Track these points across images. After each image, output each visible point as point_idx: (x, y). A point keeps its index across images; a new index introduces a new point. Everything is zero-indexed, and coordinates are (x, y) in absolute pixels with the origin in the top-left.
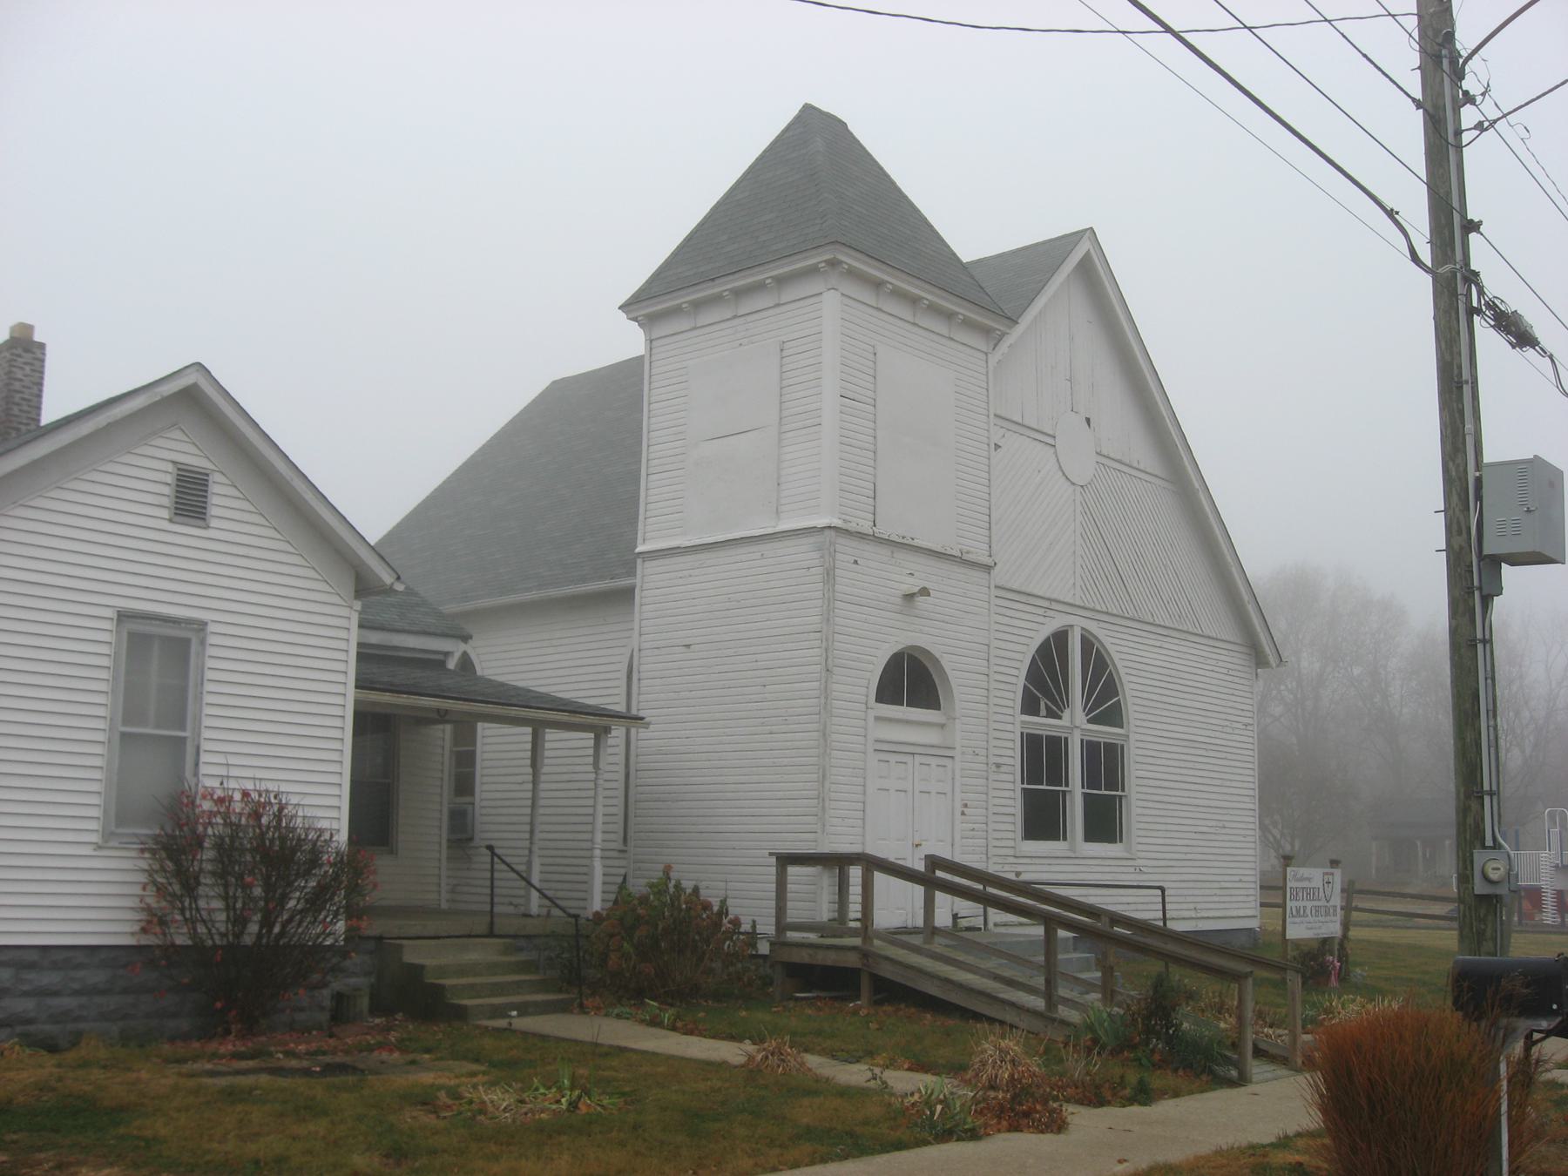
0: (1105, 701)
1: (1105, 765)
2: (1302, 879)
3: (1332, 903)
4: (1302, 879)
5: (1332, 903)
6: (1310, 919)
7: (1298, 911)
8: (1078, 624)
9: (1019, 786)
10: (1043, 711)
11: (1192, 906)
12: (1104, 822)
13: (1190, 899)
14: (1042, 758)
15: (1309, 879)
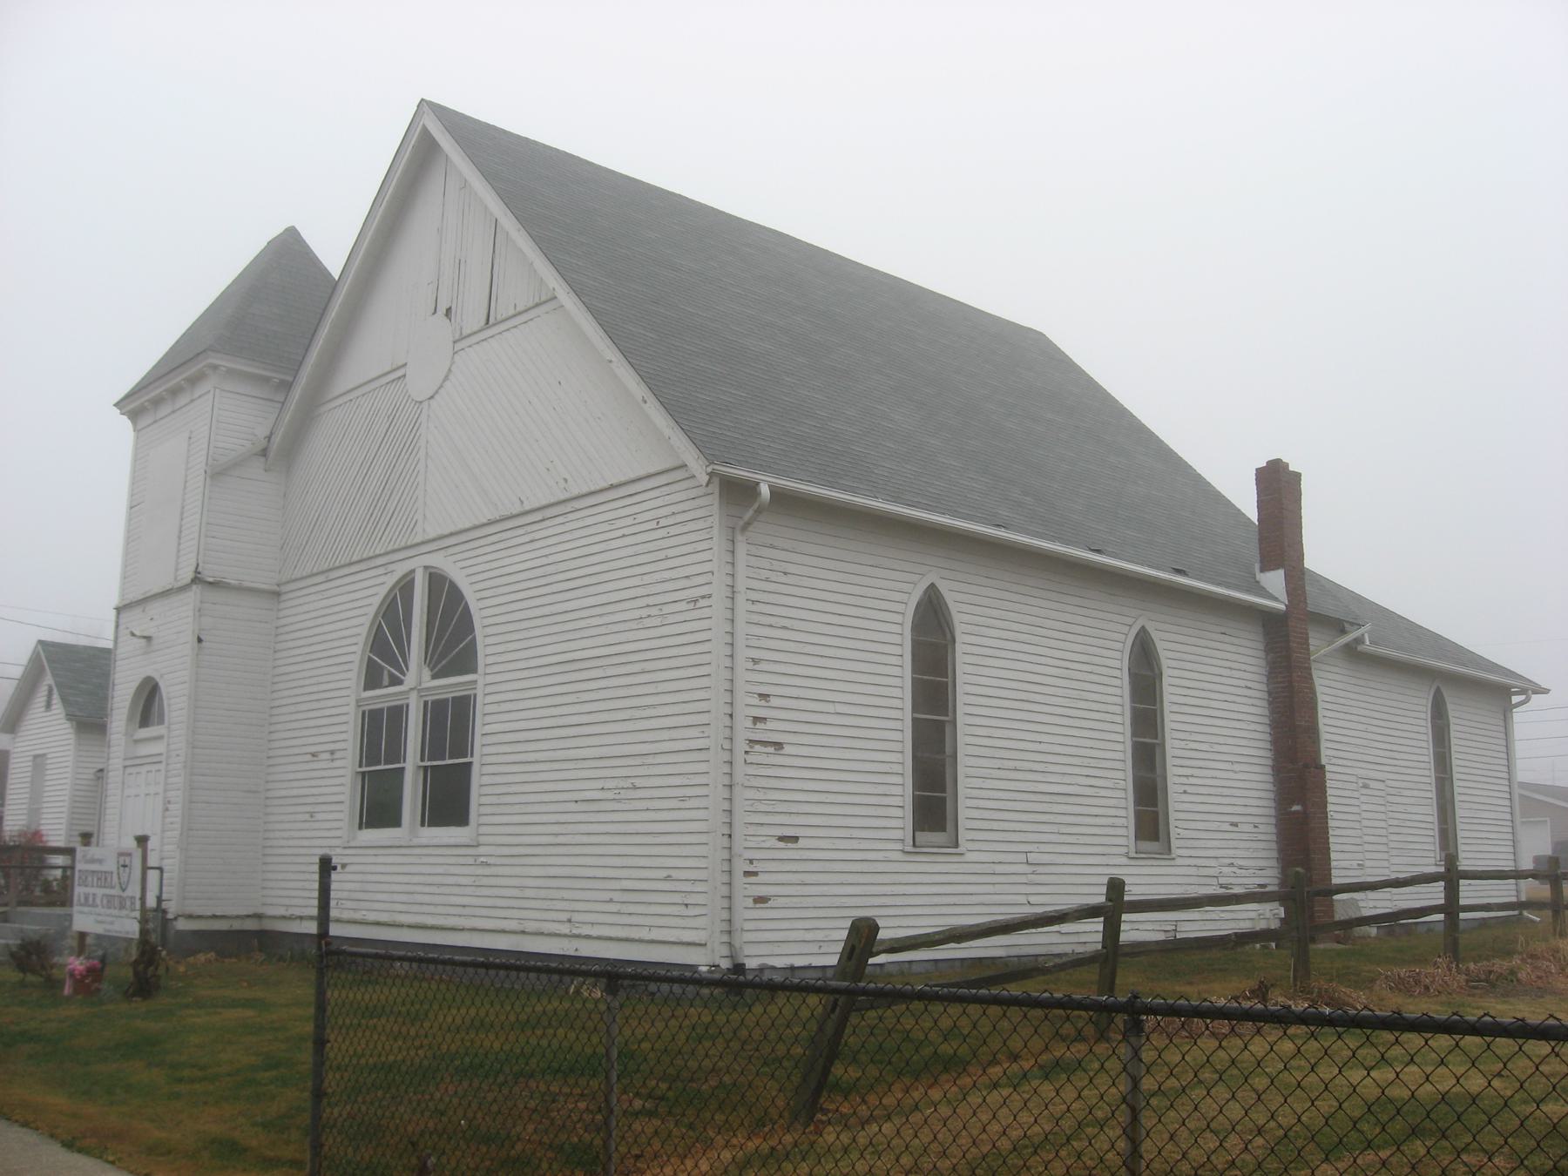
0: (454, 639)
1: (452, 724)
2: (93, 861)
3: (129, 893)
4: (93, 861)
5: (129, 893)
6: (102, 911)
7: (86, 899)
8: (418, 564)
9: (476, 760)
10: (386, 680)
11: (564, 916)
12: (449, 801)
13: (560, 905)
14: (381, 732)
15: (100, 861)
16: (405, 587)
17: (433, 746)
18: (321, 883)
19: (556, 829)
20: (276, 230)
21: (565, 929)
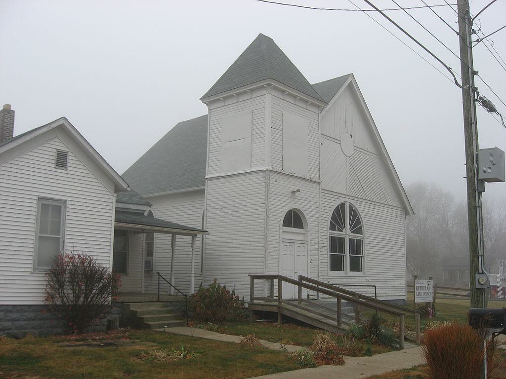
0: (357, 226)
1: (357, 246)
4: (420, 283)
8: (348, 201)
12: (356, 265)
14: (336, 244)
16: (342, 206)
17: (352, 251)
18: (253, 290)
19: (383, 274)
20: (254, 37)
21: (385, 295)
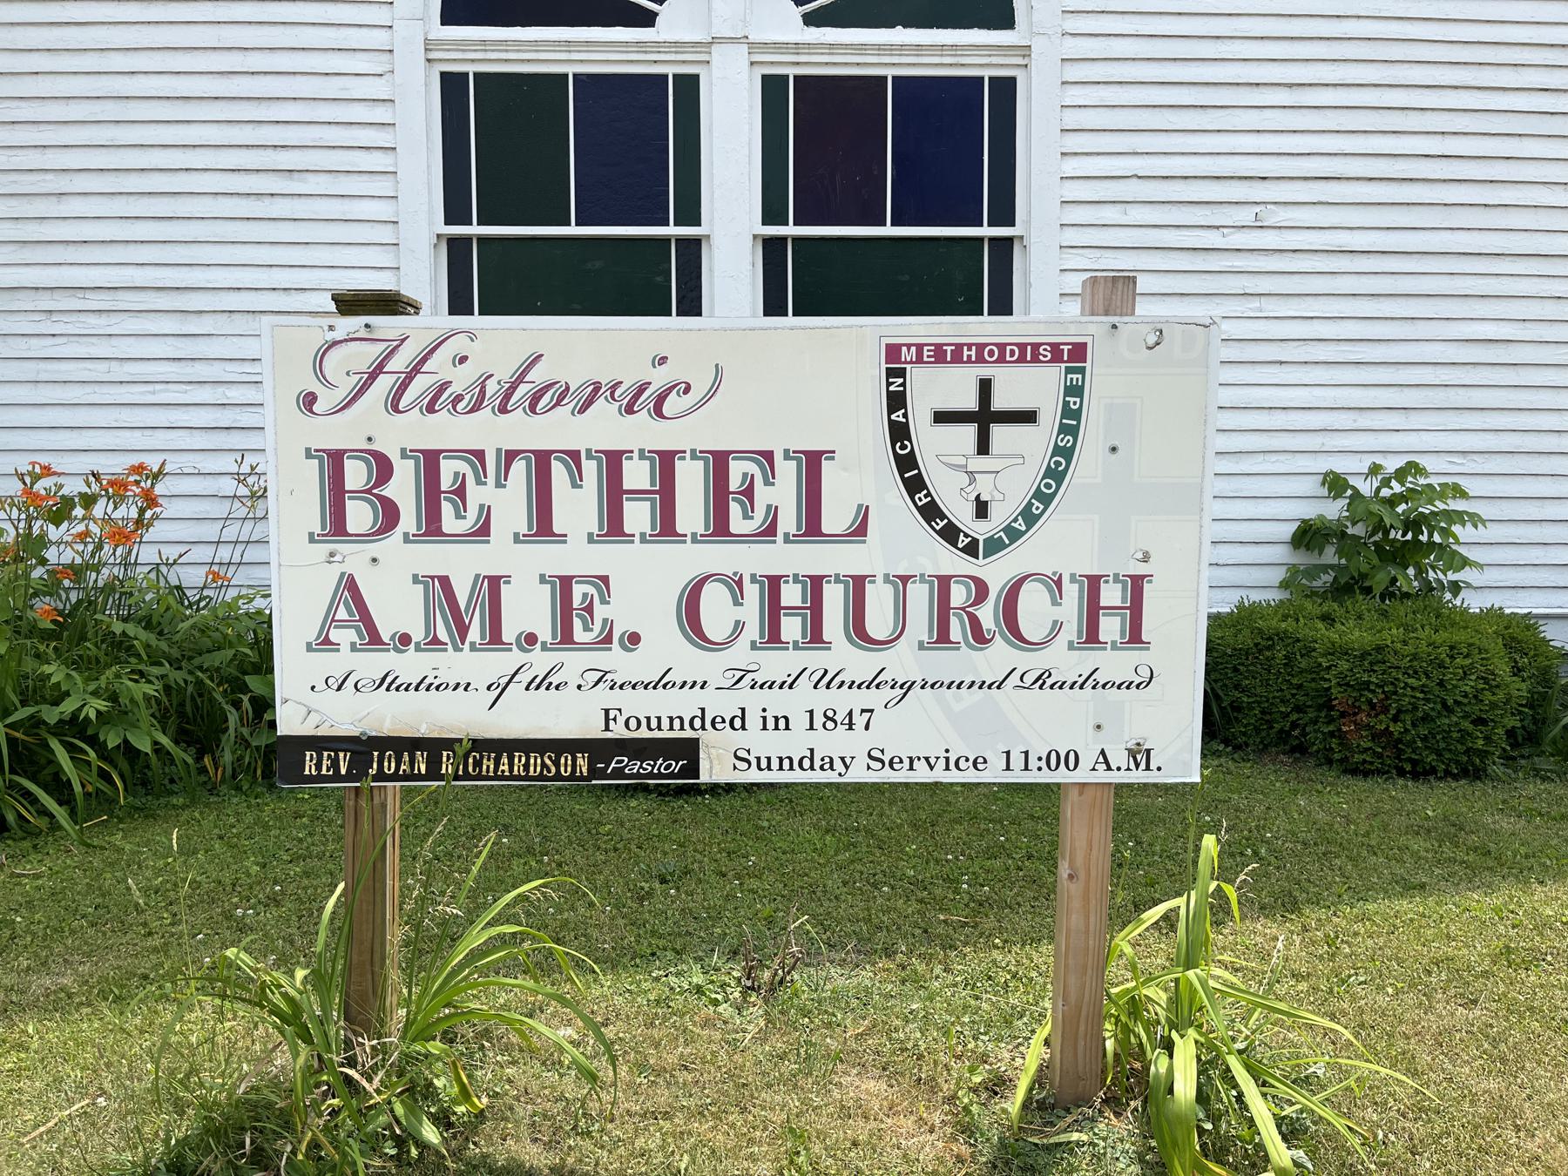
1: (953, 542)
